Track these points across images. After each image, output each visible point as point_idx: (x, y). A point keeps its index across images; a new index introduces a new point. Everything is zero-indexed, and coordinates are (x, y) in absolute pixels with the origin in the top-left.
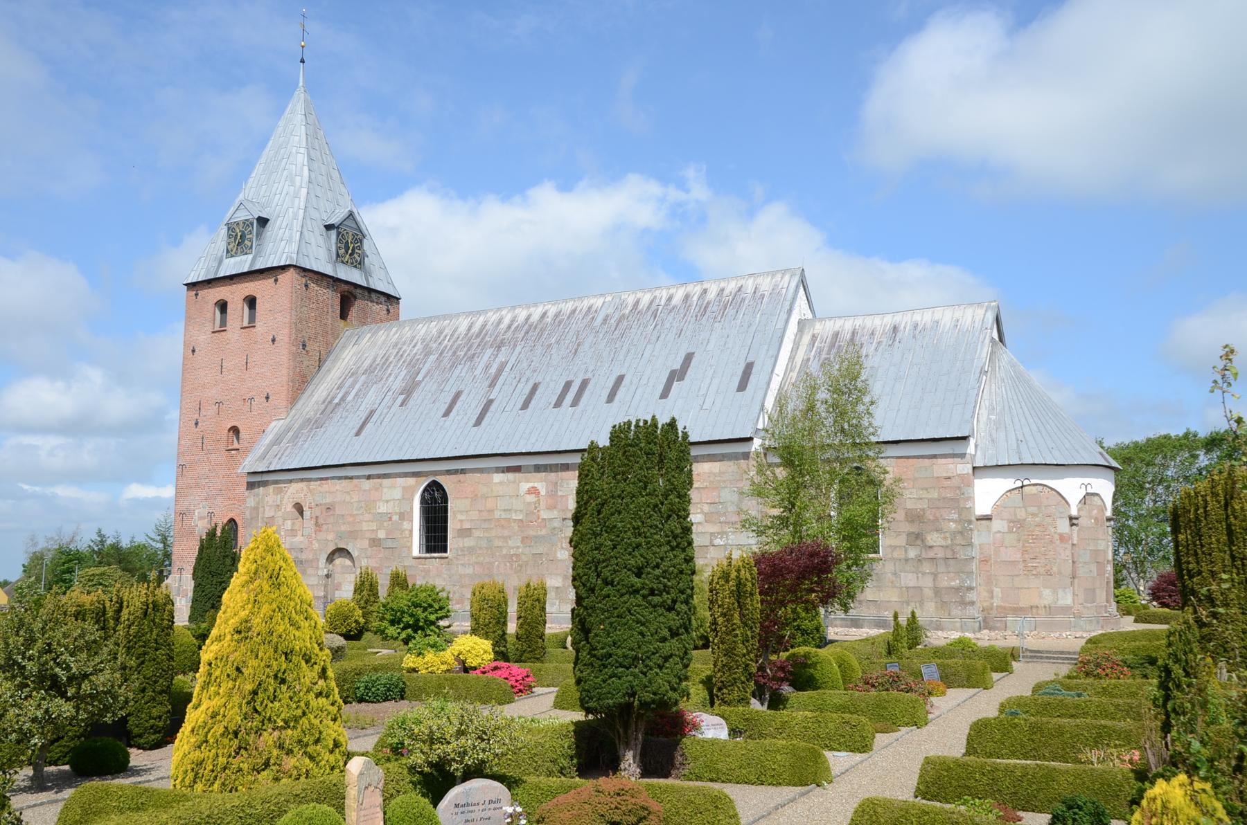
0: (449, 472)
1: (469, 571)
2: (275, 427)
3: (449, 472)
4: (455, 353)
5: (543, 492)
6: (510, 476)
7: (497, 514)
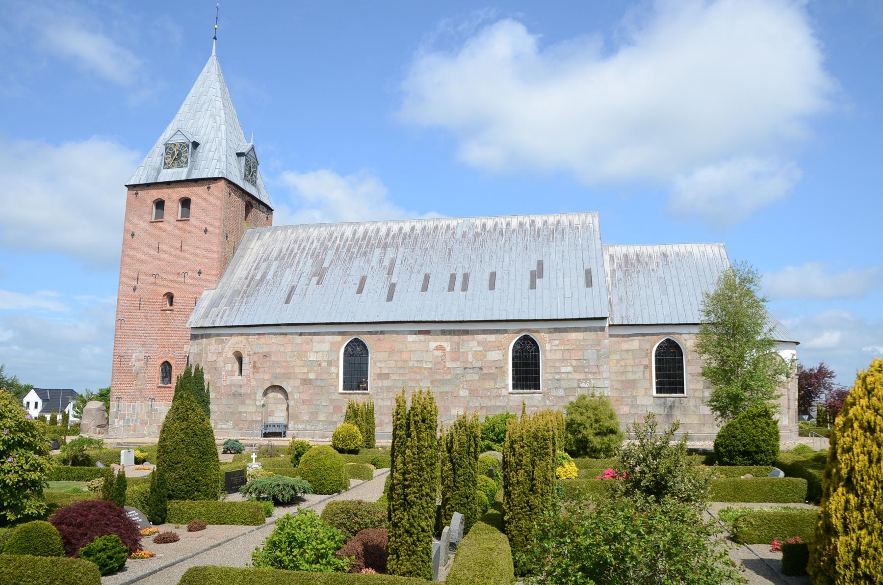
0: (370, 333)
3: (370, 333)
4: (348, 250)
5: (448, 349)
6: (422, 337)
7: (410, 364)
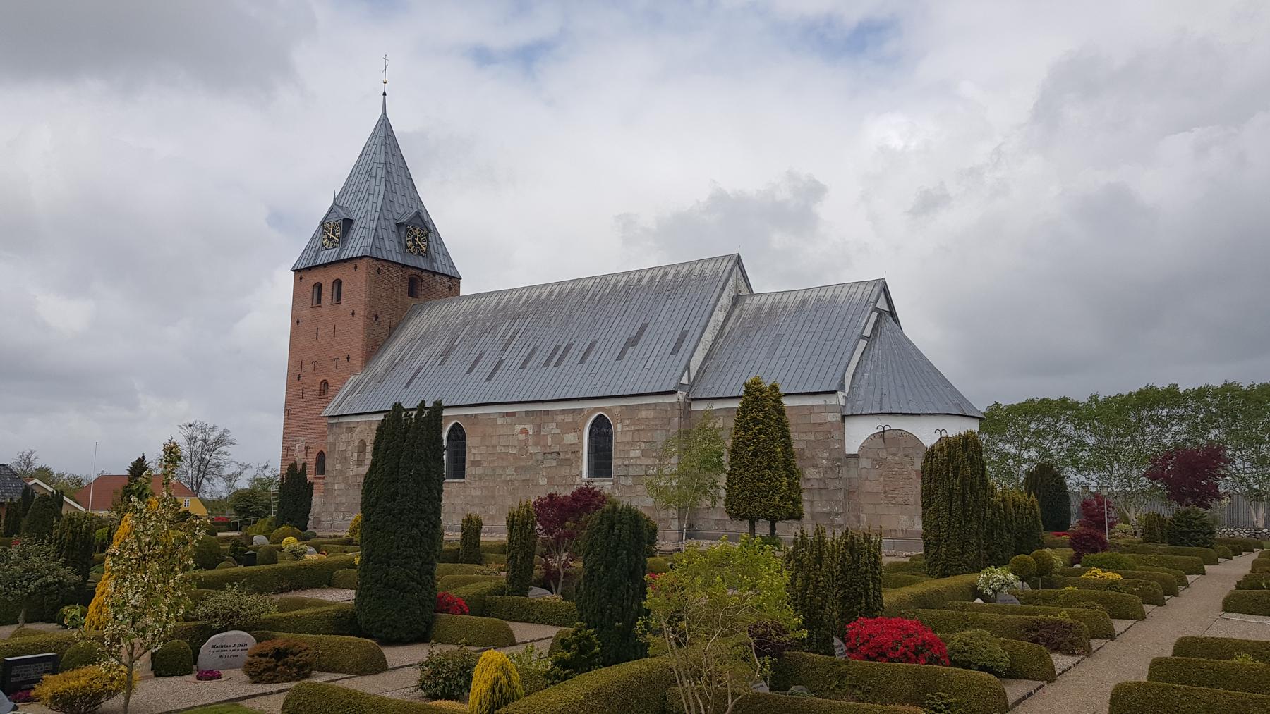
1: (479, 493)
2: (353, 379)
7: (499, 449)
